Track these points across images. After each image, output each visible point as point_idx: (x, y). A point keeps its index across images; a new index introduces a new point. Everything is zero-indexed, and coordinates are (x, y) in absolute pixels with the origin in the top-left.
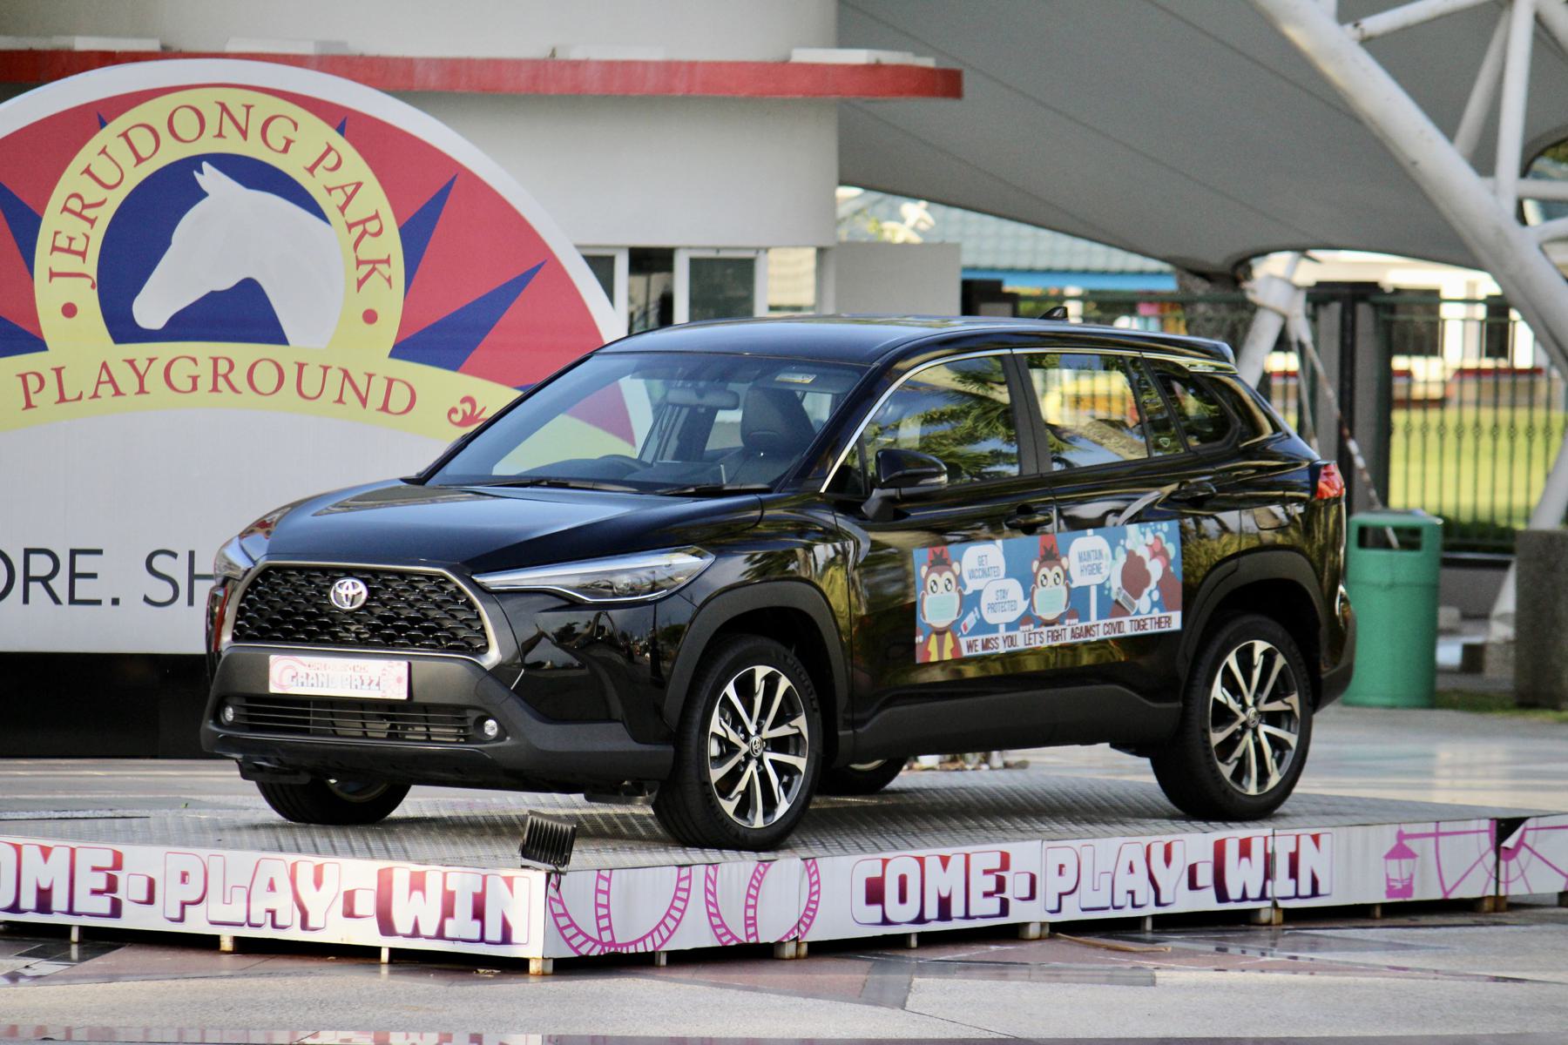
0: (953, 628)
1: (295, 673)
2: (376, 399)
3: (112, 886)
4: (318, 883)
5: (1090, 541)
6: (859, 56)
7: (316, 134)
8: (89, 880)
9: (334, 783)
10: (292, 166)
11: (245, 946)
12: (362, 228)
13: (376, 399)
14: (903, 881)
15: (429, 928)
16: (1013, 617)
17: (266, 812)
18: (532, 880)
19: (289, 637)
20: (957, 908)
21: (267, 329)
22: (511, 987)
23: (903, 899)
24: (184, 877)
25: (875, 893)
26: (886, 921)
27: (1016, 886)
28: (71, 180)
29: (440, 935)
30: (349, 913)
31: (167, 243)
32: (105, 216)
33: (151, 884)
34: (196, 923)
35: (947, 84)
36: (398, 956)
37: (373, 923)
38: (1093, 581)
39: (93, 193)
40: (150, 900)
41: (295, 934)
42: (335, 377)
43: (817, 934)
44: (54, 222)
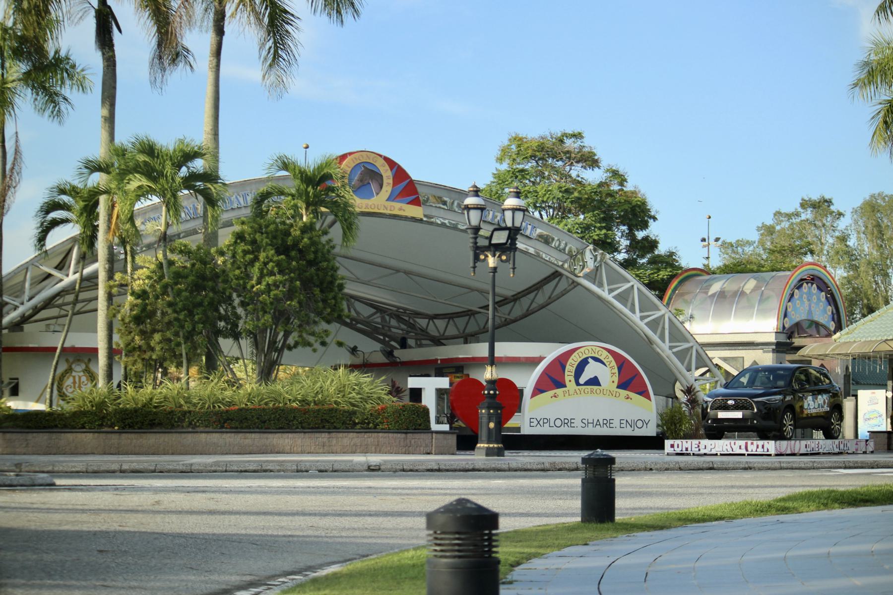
7: (606, 353)
11: (721, 455)
21: (598, 384)
28: (570, 361)
32: (575, 366)
34: (714, 452)
36: (748, 455)
44: (568, 367)
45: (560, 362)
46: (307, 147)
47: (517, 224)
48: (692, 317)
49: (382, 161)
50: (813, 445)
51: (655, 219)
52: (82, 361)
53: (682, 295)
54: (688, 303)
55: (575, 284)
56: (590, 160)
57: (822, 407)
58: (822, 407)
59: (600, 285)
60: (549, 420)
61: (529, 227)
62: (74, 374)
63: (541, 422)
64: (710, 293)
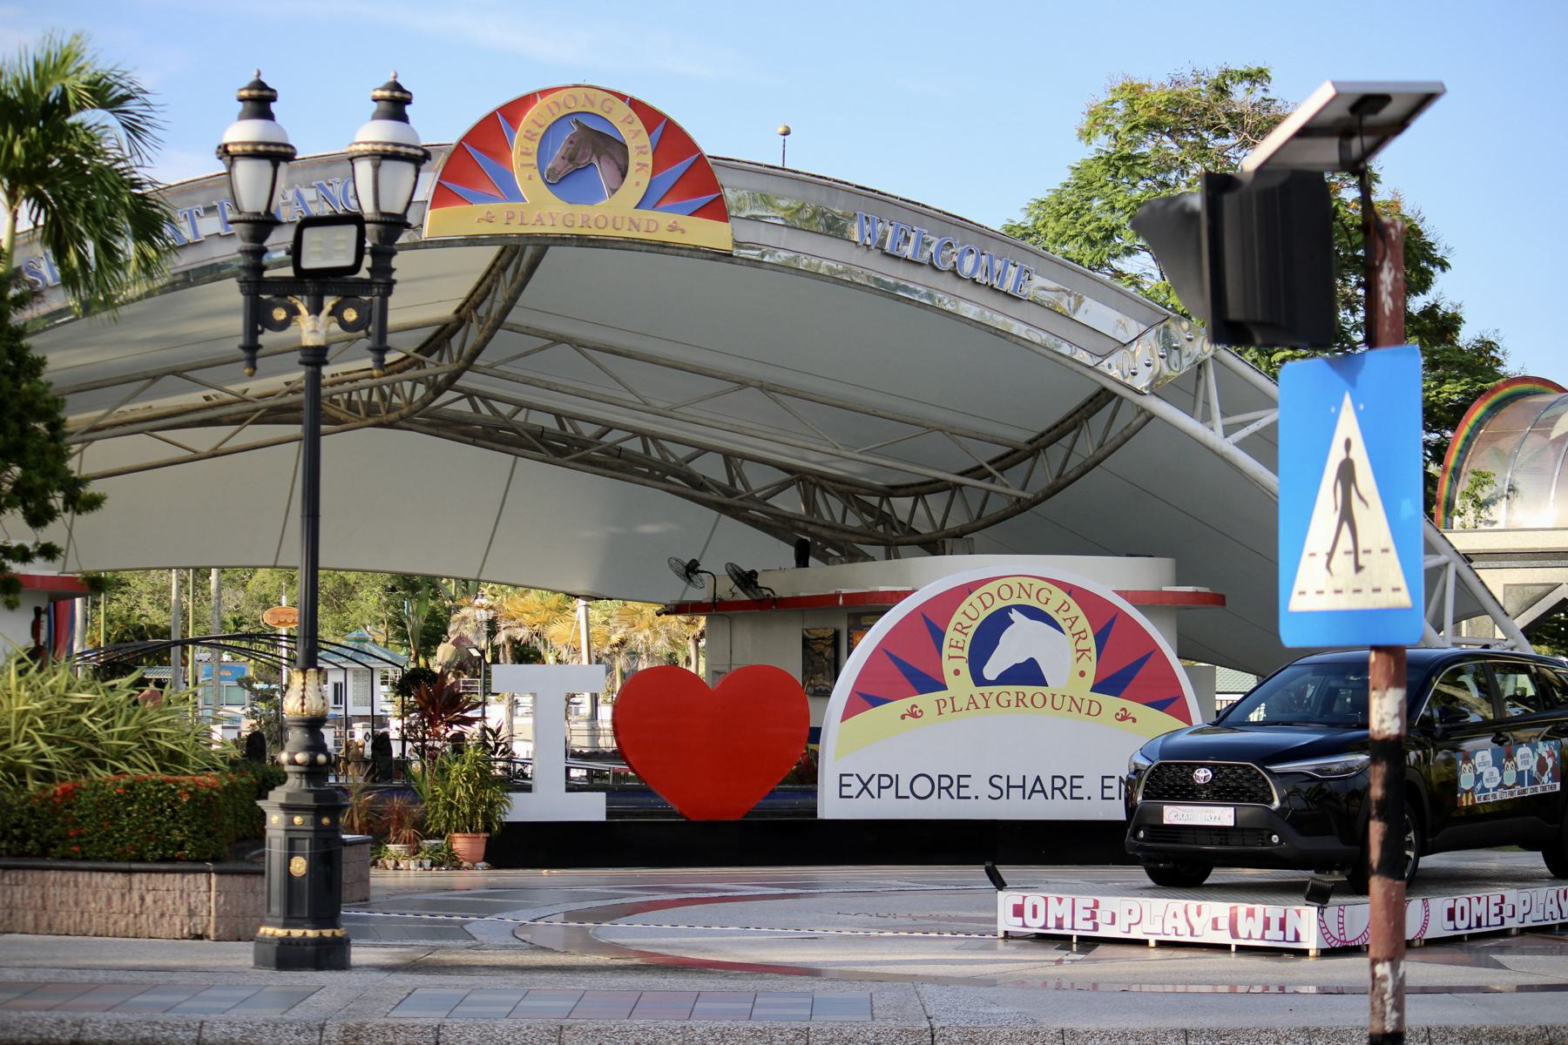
0: (1472, 790)
1: (1175, 814)
2: (1085, 710)
3: (1093, 916)
4: (1199, 914)
5: (1524, 750)
6: (1190, 589)
7: (1060, 596)
8: (1081, 914)
9: (1182, 866)
10: (1049, 609)
11: (1161, 944)
12: (1079, 636)
13: (1085, 710)
14: (1035, 908)
15: (1257, 934)
16: (1495, 784)
17: (1150, 883)
18: (1310, 912)
19: (1172, 797)
20: (1484, 923)
22: (1304, 962)
23: (1035, 916)
24: (1130, 911)
25: (1451, 915)
26: (1024, 926)
27: (1507, 911)
28: (957, 617)
29: (1263, 938)
30: (1215, 928)
31: (997, 643)
32: (971, 632)
33: (1113, 915)
34: (1136, 934)
35: (1219, 600)
37: (1228, 933)
38: (1526, 768)
39: (967, 622)
40: (1113, 923)
41: (1187, 938)
42: (1068, 700)
43: (1428, 936)
44: (950, 635)
45: (932, 621)
46: (786, 133)
47: (394, 205)
48: (1512, 489)
50: (1478, 909)
51: (1443, 265)
53: (1493, 438)
54: (1505, 458)
57: (1534, 781)
58: (1534, 781)
59: (1206, 418)
60: (894, 781)
61: (1013, 271)
63: (873, 786)
64: (1555, 434)
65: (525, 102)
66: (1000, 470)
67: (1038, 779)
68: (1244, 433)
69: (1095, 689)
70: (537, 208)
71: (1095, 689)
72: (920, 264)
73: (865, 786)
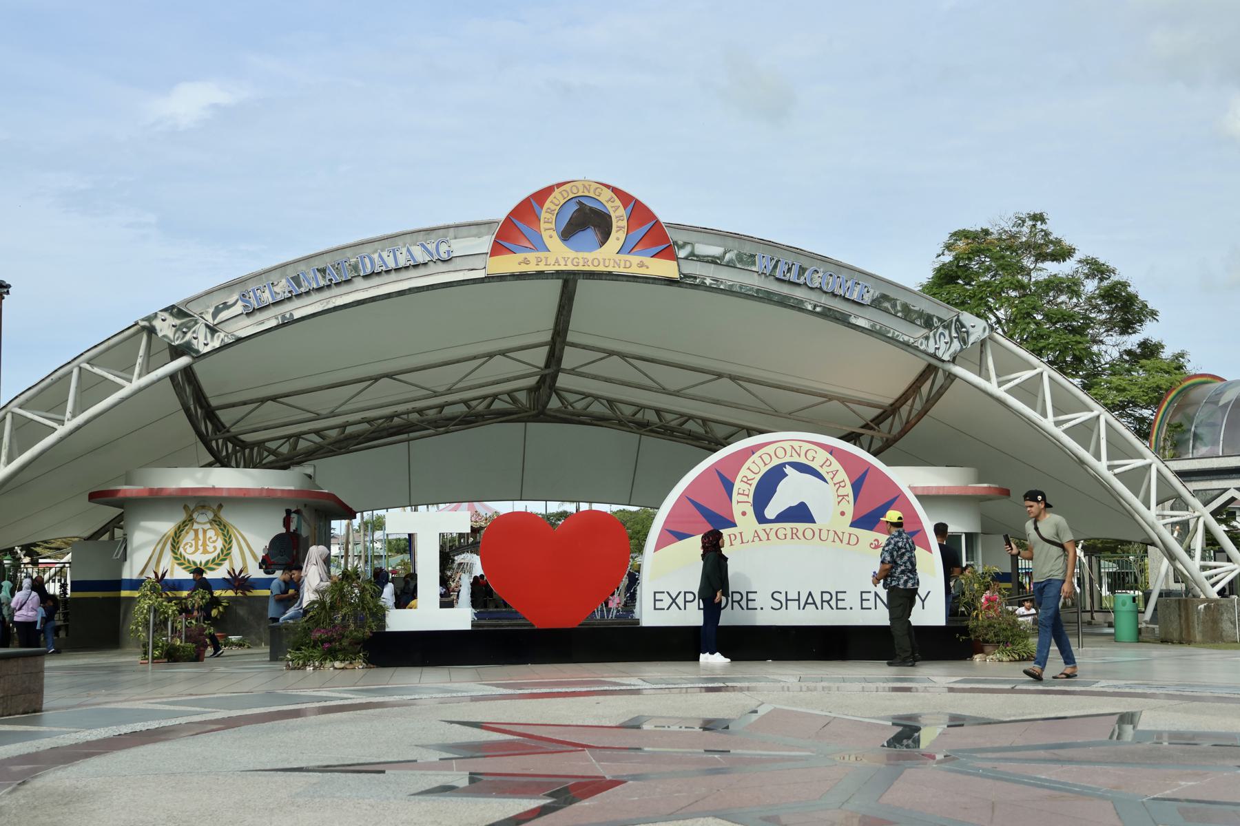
7: (823, 455)
12: (839, 485)
13: (846, 540)
28: (744, 471)
32: (755, 483)
39: (751, 476)
42: (832, 534)
44: (738, 485)
49: (609, 193)
52: (210, 508)
55: (951, 377)
56: (1062, 254)
59: (988, 379)
62: (196, 526)
63: (680, 601)
64: (1221, 403)
65: (548, 191)
66: (877, 425)
67: (810, 594)
68: (1066, 426)
69: (853, 525)
70: (560, 255)
71: (853, 525)
72: (798, 285)
73: (674, 601)
